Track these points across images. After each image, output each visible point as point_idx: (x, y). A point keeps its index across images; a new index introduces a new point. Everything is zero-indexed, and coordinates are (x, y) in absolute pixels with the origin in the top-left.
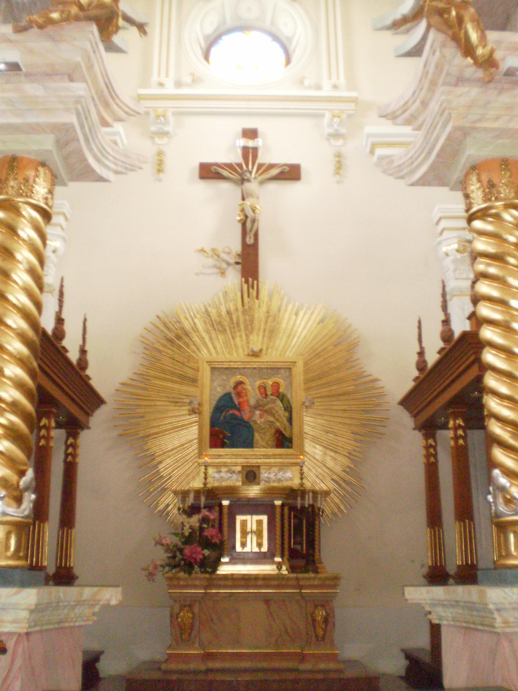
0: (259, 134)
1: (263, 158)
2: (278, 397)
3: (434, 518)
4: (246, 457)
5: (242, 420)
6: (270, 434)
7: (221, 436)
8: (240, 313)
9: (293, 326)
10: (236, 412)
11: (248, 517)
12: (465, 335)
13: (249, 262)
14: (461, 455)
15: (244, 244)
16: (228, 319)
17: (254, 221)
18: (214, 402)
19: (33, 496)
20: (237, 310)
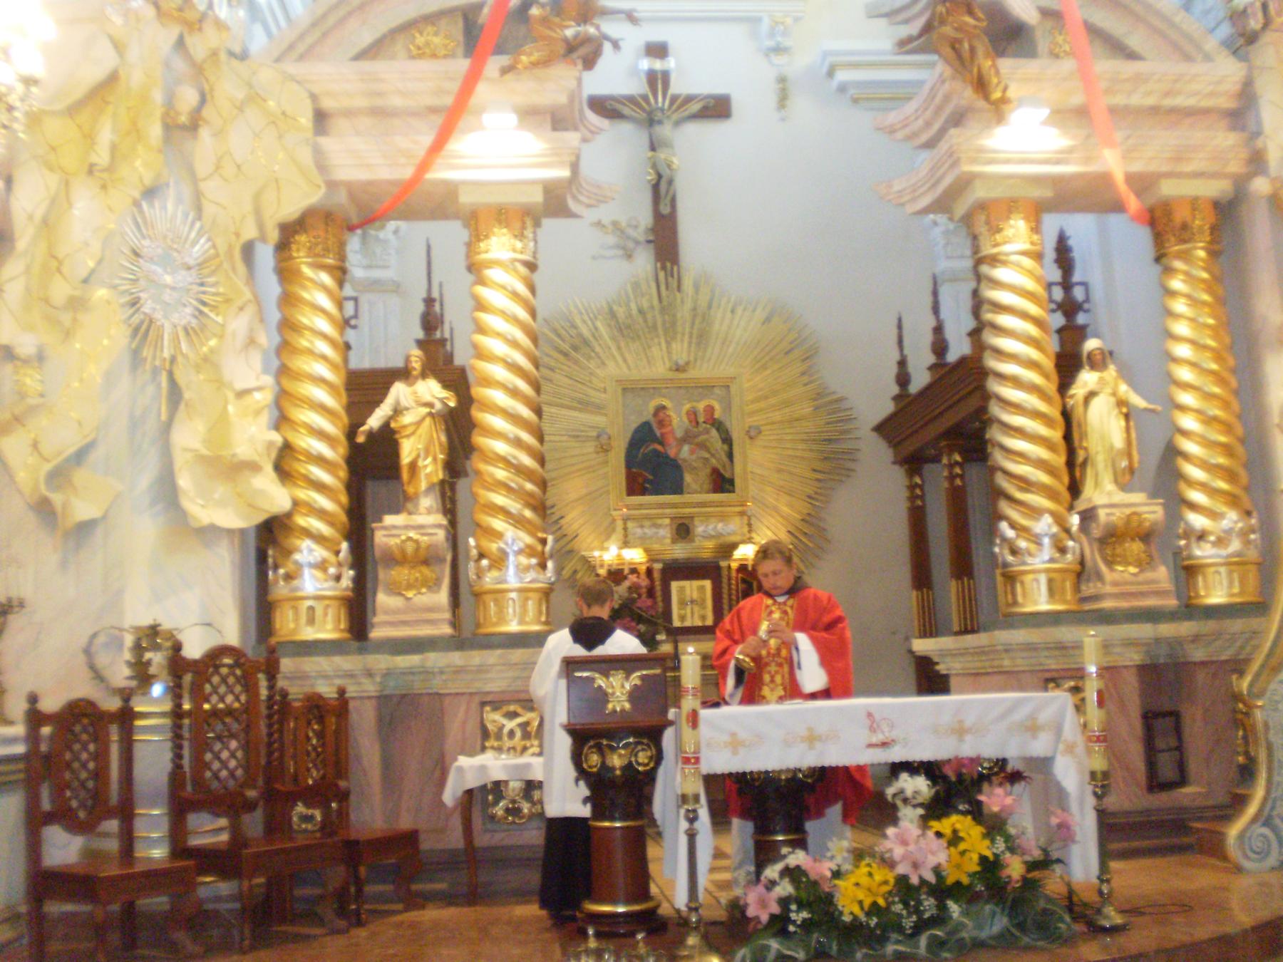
0: (671, 50)
1: (679, 86)
2: (713, 425)
3: (922, 577)
4: (674, 506)
5: (667, 457)
6: (705, 473)
7: (640, 480)
8: (657, 313)
9: (729, 328)
10: (659, 448)
11: (686, 583)
12: (963, 361)
13: (664, 239)
14: (958, 499)
15: (658, 216)
16: (641, 320)
17: (670, 182)
18: (629, 435)
19: (351, 573)
20: (652, 307)
